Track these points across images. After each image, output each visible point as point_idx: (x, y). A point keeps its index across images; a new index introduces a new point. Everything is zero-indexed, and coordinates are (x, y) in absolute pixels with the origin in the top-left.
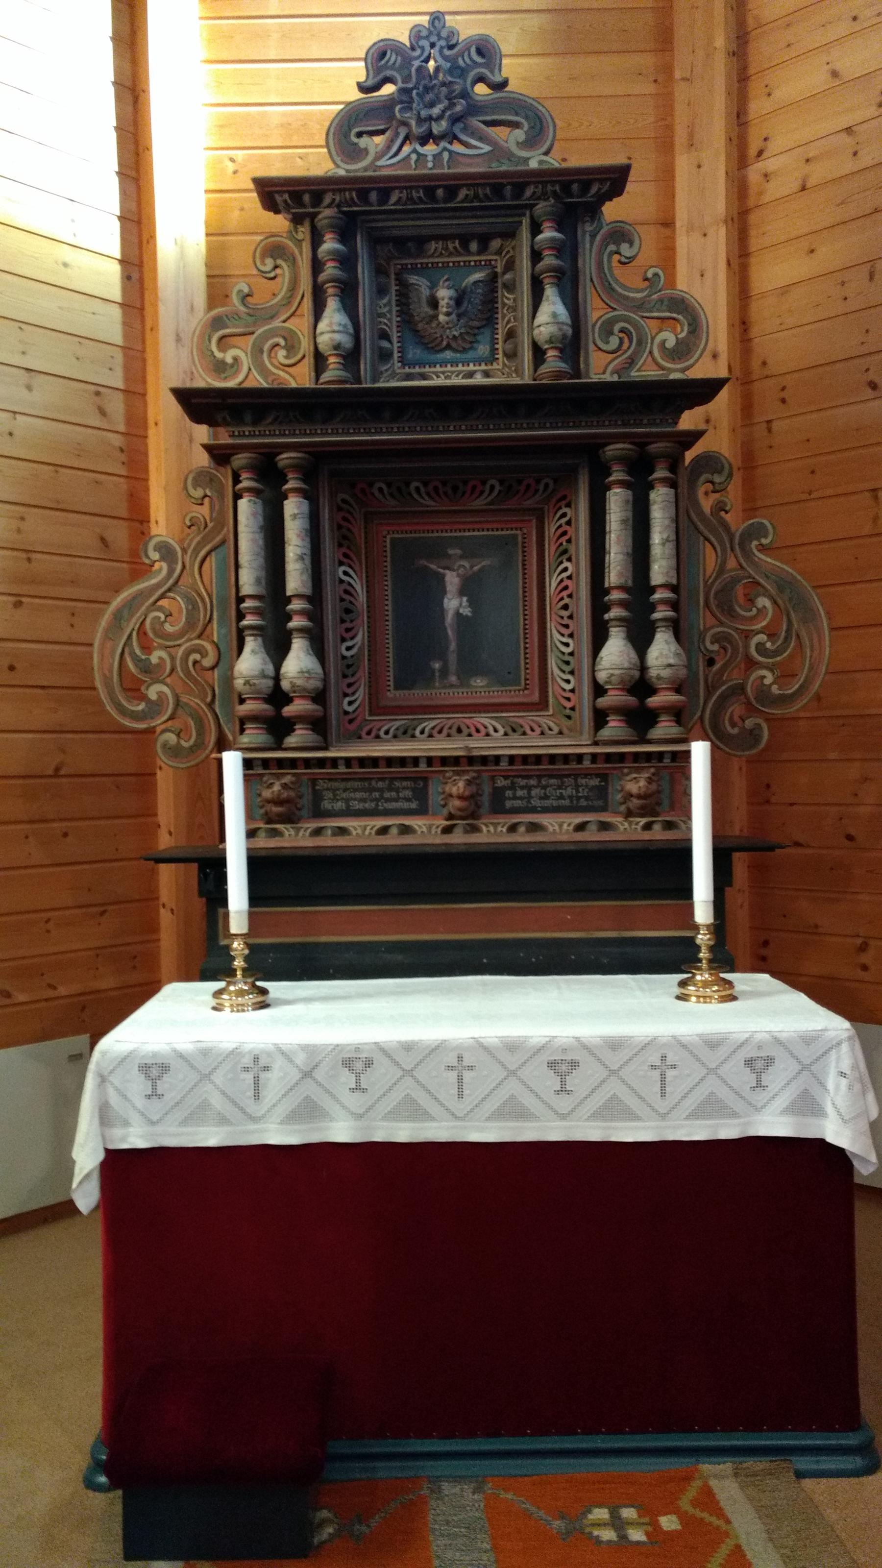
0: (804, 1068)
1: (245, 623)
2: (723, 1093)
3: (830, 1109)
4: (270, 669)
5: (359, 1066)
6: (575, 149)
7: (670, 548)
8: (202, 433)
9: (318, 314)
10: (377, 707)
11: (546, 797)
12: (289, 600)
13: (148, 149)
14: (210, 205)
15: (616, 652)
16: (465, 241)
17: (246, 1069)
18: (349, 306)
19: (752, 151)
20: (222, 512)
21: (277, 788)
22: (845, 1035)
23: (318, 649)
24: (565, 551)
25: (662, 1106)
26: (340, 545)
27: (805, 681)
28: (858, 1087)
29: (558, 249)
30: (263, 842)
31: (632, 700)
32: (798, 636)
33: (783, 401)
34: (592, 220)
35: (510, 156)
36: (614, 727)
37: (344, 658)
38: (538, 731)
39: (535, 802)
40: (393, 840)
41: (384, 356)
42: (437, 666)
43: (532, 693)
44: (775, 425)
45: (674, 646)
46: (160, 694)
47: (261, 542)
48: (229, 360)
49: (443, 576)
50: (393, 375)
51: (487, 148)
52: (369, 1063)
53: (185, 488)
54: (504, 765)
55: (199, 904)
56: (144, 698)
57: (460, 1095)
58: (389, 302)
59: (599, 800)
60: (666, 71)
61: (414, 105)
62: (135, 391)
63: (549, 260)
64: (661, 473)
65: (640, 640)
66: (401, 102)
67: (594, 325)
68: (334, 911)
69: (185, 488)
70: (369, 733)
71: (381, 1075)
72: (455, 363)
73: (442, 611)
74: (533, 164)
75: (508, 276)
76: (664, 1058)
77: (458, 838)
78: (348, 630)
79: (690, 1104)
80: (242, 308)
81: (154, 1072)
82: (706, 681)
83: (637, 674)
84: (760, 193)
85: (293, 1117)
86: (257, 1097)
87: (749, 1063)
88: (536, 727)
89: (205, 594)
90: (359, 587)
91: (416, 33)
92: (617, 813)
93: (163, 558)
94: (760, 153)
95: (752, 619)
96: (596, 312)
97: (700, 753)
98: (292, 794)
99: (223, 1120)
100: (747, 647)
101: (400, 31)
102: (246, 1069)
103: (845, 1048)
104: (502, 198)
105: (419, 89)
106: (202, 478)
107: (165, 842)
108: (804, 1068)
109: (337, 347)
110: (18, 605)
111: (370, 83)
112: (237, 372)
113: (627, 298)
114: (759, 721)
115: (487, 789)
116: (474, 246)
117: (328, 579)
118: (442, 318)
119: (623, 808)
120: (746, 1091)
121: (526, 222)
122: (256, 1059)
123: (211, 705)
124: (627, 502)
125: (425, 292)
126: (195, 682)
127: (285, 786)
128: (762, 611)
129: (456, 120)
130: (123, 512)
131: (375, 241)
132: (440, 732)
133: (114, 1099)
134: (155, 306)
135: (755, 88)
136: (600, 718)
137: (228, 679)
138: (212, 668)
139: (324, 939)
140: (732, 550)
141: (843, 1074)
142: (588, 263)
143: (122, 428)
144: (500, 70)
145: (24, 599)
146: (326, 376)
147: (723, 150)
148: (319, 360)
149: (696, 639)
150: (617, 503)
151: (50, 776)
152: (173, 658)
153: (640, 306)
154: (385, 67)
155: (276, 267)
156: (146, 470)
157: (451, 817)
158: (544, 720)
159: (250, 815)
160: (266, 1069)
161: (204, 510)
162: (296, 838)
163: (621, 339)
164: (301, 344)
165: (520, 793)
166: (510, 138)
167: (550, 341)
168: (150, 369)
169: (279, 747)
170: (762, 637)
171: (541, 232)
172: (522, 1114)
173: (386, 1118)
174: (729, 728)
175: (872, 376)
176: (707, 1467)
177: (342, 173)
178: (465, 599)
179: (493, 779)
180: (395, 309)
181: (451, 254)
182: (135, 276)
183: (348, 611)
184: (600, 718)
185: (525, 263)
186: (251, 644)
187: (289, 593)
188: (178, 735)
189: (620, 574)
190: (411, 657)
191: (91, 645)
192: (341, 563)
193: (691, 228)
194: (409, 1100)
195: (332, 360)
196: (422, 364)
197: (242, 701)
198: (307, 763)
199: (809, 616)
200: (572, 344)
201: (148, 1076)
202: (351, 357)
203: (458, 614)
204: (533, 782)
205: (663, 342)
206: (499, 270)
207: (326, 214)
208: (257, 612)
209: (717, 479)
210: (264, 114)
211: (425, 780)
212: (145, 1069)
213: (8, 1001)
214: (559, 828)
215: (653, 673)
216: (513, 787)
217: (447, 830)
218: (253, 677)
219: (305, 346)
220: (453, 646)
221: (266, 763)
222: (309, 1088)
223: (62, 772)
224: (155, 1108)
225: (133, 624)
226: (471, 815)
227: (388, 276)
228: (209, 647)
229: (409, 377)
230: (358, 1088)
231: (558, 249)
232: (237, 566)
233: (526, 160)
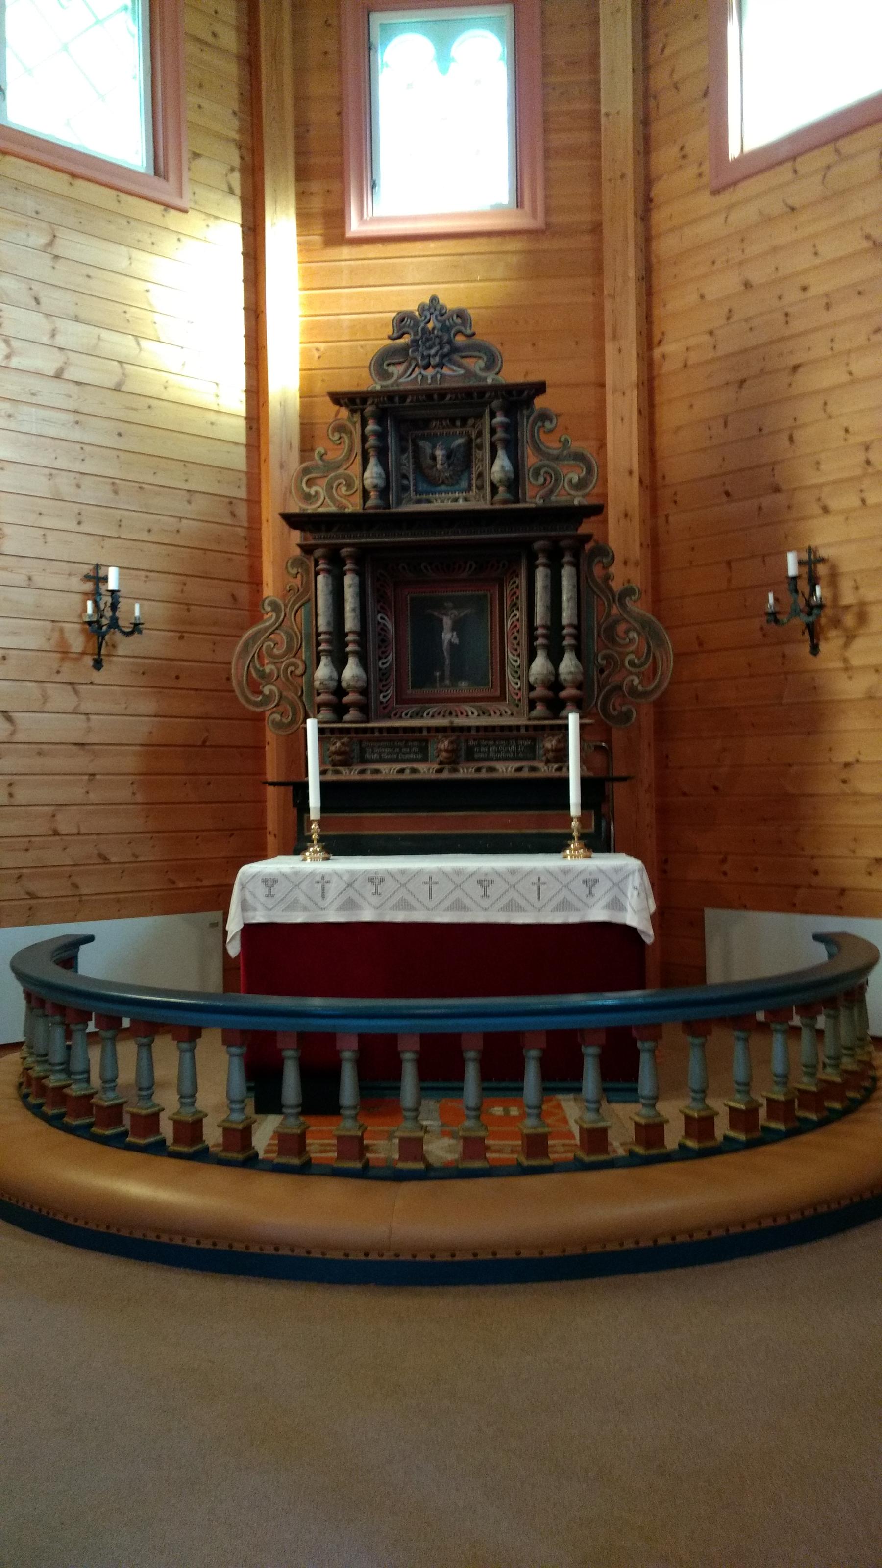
0: (615, 885)
1: (321, 648)
2: (571, 898)
3: (629, 908)
4: (335, 675)
5: (377, 881)
6: (512, 373)
7: (573, 603)
8: (296, 536)
9: (364, 469)
10: (401, 699)
11: (499, 752)
12: (346, 635)
13: (265, 347)
14: (302, 378)
15: (540, 665)
16: (453, 421)
17: (318, 882)
18: (383, 461)
19: (656, 340)
20: (308, 582)
21: (338, 744)
22: (637, 868)
23: (364, 662)
24: (515, 604)
25: (538, 905)
26: (379, 601)
27: (659, 682)
28: (643, 895)
29: (506, 427)
30: (330, 777)
31: (549, 694)
32: (654, 657)
33: (675, 502)
34: (528, 408)
35: (475, 376)
36: (540, 709)
37: (380, 669)
38: (498, 713)
39: (492, 754)
40: (407, 776)
41: (405, 489)
42: (438, 674)
43: (496, 691)
44: (671, 519)
45: (575, 661)
46: (271, 691)
47: (330, 601)
48: (313, 492)
49: (442, 620)
50: (410, 501)
51: (462, 372)
52: (382, 880)
53: (287, 568)
54: (473, 732)
55: (293, 813)
56: (261, 693)
57: (431, 897)
58: (408, 457)
59: (531, 753)
60: (598, 290)
61: (420, 349)
62: (254, 500)
63: (500, 434)
64: (567, 558)
65: (555, 658)
66: (412, 346)
67: (529, 471)
68: (363, 816)
69: (287, 568)
70: (395, 715)
71: (390, 886)
72: (447, 492)
73: (441, 642)
74: (489, 381)
75: (479, 441)
76: (539, 879)
77: (445, 775)
78: (383, 652)
79: (554, 903)
80: (320, 462)
81: (270, 883)
82: (599, 683)
83: (552, 678)
84: (661, 367)
85: (342, 908)
86: (323, 896)
87: (585, 882)
88: (497, 711)
89: (296, 630)
90: (390, 626)
91: (422, 308)
92: (540, 761)
93: (273, 610)
94: (660, 342)
95: (627, 645)
96: (531, 459)
97: (573, 720)
98: (347, 749)
99: (305, 909)
100: (623, 661)
101: (412, 306)
102: (318, 882)
103: (637, 874)
104: (472, 398)
105: (424, 339)
106: (297, 562)
107: (271, 776)
108: (615, 885)
109: (375, 486)
110: (181, 638)
111: (395, 335)
112: (317, 500)
113: (549, 454)
114: (630, 706)
115: (463, 746)
116: (458, 423)
117: (370, 620)
118: (439, 466)
119: (544, 758)
120: (584, 898)
121: (487, 411)
122: (323, 877)
123: (301, 697)
124: (546, 576)
125: (429, 451)
126: (292, 683)
127: (343, 744)
128: (632, 641)
129: (443, 356)
130: (246, 578)
131: (399, 422)
132: (439, 714)
133: (249, 897)
134: (267, 444)
135: (656, 300)
136: (532, 704)
137: (311, 681)
138: (302, 675)
139: (366, 833)
140: (614, 601)
141: (635, 888)
142: (525, 432)
143: (246, 524)
144: (471, 327)
145: (185, 634)
146: (370, 503)
147: (634, 339)
148: (365, 494)
149: (592, 657)
150: (541, 576)
151: (199, 746)
152: (278, 670)
153: (557, 458)
154: (404, 326)
155: (340, 438)
156: (261, 551)
157: (441, 763)
158: (503, 707)
159: (322, 761)
160: (328, 882)
161: (298, 581)
162: (350, 774)
163: (545, 480)
164: (352, 485)
165: (482, 749)
166: (476, 365)
167: (500, 481)
168: (263, 485)
169: (340, 720)
170: (632, 656)
171: (495, 417)
172: (464, 908)
173: (391, 909)
174: (612, 711)
175: (728, 488)
176: (560, 1097)
177: (378, 387)
178: (455, 633)
179: (467, 741)
180: (411, 460)
181: (444, 428)
182: (255, 426)
183: (383, 641)
184: (532, 704)
185: (487, 435)
186: (324, 660)
187: (347, 630)
188: (281, 715)
189: (542, 619)
190: (423, 670)
191: (230, 663)
192: (379, 612)
193: (615, 390)
194: (403, 900)
195: (372, 494)
196: (428, 493)
197: (319, 694)
198: (357, 730)
199: (661, 643)
200: (514, 483)
201: (266, 886)
202: (384, 492)
203: (451, 643)
204: (491, 743)
205: (571, 481)
206: (473, 436)
207: (369, 409)
208: (327, 641)
209: (605, 560)
210: (339, 320)
211: (427, 741)
212: (265, 881)
213: (172, 886)
214: (506, 769)
215: (562, 677)
216: (479, 745)
217: (439, 771)
218: (326, 680)
219: (357, 483)
220: (447, 662)
221: (332, 731)
222: (351, 893)
223: (207, 744)
224: (270, 902)
225: (254, 649)
226: (453, 761)
227: (407, 441)
228: (300, 663)
229: (419, 502)
230: (376, 893)
231: (506, 427)
232: (317, 615)
233: (485, 379)
